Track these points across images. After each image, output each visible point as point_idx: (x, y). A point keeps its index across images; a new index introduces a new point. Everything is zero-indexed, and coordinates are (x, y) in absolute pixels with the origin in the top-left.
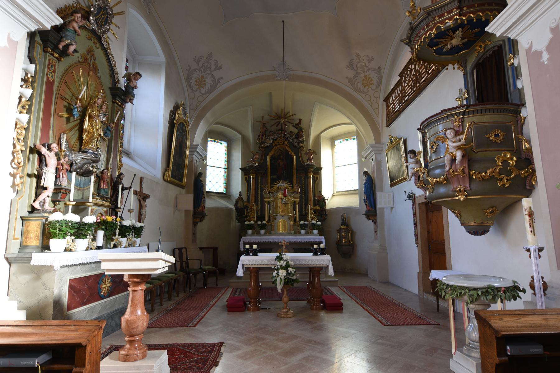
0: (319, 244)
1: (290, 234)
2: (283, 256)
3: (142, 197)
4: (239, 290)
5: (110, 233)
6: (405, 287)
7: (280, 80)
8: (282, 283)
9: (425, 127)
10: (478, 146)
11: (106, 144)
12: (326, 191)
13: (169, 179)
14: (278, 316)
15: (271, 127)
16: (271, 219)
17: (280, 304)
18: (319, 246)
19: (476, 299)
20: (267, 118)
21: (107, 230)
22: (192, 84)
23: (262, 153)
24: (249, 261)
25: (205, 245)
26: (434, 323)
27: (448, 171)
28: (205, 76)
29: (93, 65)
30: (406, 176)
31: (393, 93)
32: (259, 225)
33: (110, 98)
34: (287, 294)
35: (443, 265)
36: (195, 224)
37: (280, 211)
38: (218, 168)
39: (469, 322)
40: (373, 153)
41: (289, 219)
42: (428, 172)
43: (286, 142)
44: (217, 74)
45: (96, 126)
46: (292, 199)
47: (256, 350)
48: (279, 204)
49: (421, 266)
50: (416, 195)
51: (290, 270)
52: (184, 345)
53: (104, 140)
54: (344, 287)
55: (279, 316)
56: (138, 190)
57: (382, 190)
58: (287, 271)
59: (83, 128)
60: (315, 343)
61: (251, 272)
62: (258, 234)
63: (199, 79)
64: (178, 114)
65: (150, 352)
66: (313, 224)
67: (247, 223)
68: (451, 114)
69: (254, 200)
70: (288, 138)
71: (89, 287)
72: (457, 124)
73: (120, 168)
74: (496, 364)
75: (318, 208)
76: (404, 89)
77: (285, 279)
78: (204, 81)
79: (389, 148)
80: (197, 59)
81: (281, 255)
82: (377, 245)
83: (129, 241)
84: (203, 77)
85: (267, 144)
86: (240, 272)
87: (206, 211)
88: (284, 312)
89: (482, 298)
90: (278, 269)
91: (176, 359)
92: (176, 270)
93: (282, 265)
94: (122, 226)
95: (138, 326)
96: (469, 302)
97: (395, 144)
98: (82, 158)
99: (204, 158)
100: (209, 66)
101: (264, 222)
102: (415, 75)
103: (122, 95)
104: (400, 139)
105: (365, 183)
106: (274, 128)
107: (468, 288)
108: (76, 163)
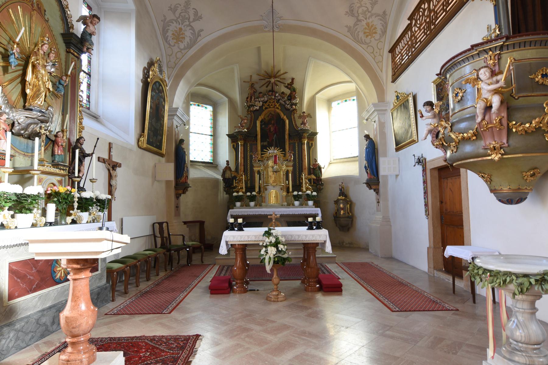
0: (314, 216)
1: (282, 206)
2: (272, 231)
3: (112, 166)
4: (226, 267)
5: (65, 206)
6: (412, 263)
7: (269, 31)
8: (272, 262)
9: (447, 71)
10: (519, 90)
11: (60, 101)
12: (322, 159)
13: (145, 145)
14: (267, 299)
15: (260, 87)
16: (262, 190)
17: (269, 285)
18: (314, 219)
19: (527, 289)
20: (255, 78)
21: (60, 202)
22: (169, 38)
23: (251, 118)
24: (234, 236)
25: (190, 219)
26: (452, 308)
27: (479, 123)
28: (183, 28)
29: (38, 5)
30: (415, 137)
31: (400, 42)
32: (248, 196)
33: (62, 47)
34: (277, 275)
35: (460, 241)
36: (178, 196)
37: (271, 181)
38: (204, 135)
39: (508, 318)
40: (376, 113)
41: (281, 189)
42: (451, 127)
43: (277, 105)
44: (197, 25)
45: (42, 78)
46: (284, 168)
47: (238, 344)
48: (270, 173)
49: (432, 241)
50: (427, 160)
51: (281, 247)
52: (153, 339)
53: (56, 96)
54: (344, 264)
55: (268, 299)
56: (106, 157)
57: (385, 155)
58: (277, 249)
59: (26, 81)
60: (311, 335)
61: (236, 249)
62: (248, 206)
63: (176, 31)
64: (153, 71)
65: (99, 354)
66: (308, 195)
67: (235, 194)
68: (484, 50)
69: (243, 169)
70: (279, 100)
71: (38, 271)
72: (492, 62)
73: (80, 132)
74: (62, 34)
75: (313, 177)
76: (414, 35)
77: (274, 258)
78: (183, 34)
79: (395, 106)
80: (173, 7)
81: (270, 229)
82: (379, 217)
83: (92, 215)
84: (181, 29)
85: (256, 108)
86: (223, 250)
87: (189, 182)
88: (274, 295)
89: (536, 288)
90: (266, 247)
91: (140, 358)
92: (156, 246)
93: (271, 242)
94: (80, 199)
95: (80, 325)
96: (517, 292)
97: (402, 103)
98: (27, 117)
99: (186, 123)
100: (187, 16)
101: (254, 193)
102: (428, 16)
103: (77, 44)
104: (408, 96)
105: (366, 149)
106: (264, 89)
107: (515, 274)
108: (19, 123)
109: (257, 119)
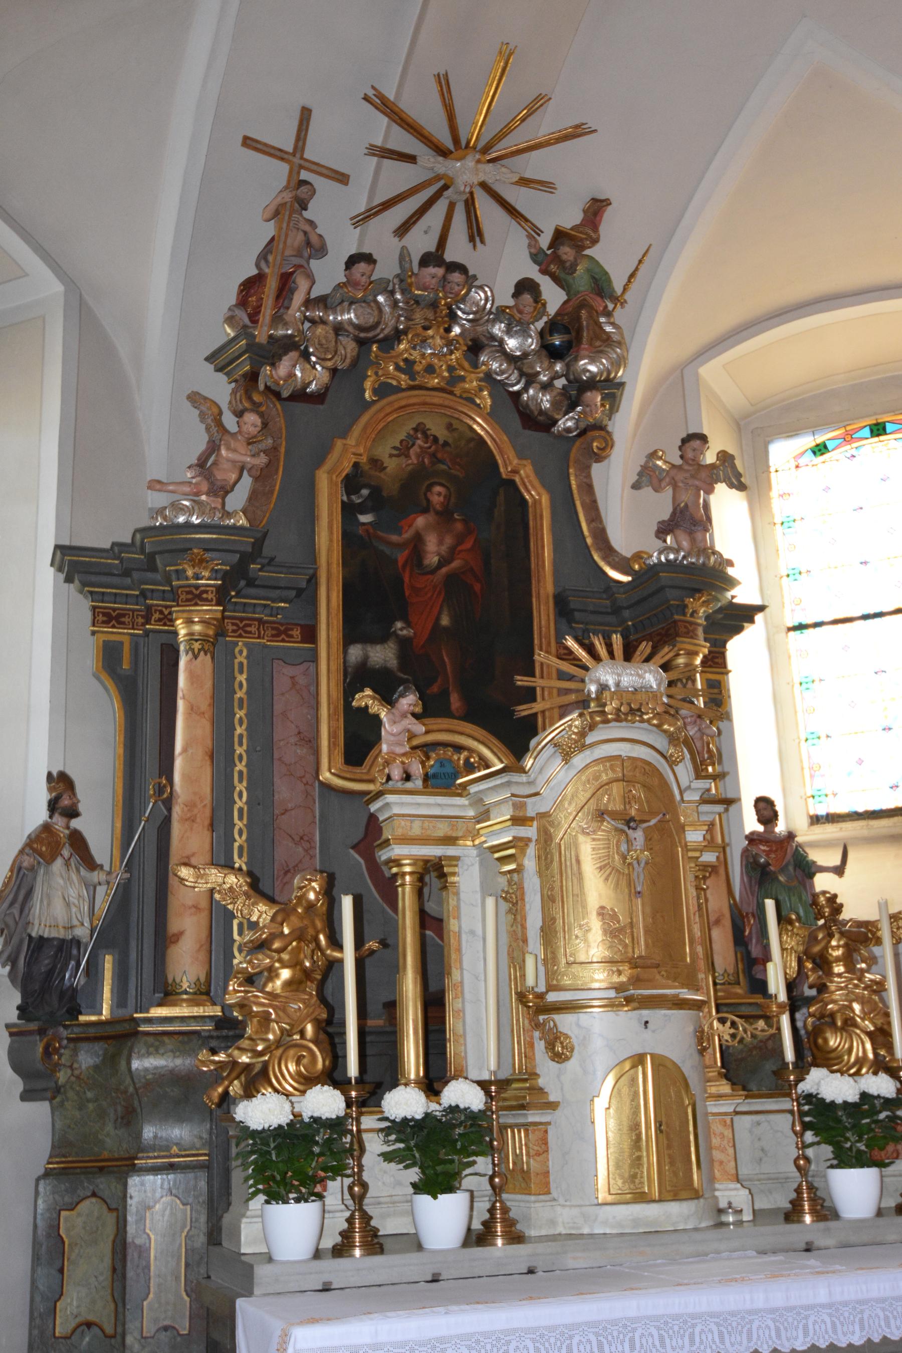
109: (319, 461)
